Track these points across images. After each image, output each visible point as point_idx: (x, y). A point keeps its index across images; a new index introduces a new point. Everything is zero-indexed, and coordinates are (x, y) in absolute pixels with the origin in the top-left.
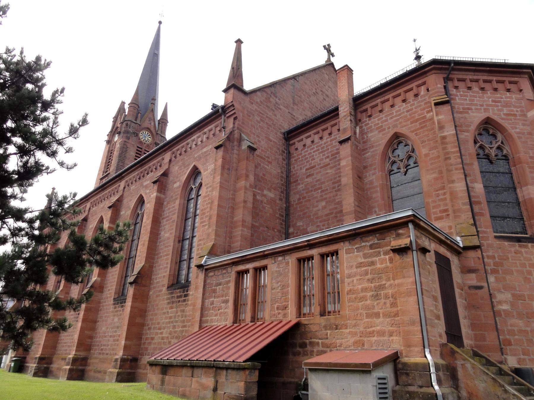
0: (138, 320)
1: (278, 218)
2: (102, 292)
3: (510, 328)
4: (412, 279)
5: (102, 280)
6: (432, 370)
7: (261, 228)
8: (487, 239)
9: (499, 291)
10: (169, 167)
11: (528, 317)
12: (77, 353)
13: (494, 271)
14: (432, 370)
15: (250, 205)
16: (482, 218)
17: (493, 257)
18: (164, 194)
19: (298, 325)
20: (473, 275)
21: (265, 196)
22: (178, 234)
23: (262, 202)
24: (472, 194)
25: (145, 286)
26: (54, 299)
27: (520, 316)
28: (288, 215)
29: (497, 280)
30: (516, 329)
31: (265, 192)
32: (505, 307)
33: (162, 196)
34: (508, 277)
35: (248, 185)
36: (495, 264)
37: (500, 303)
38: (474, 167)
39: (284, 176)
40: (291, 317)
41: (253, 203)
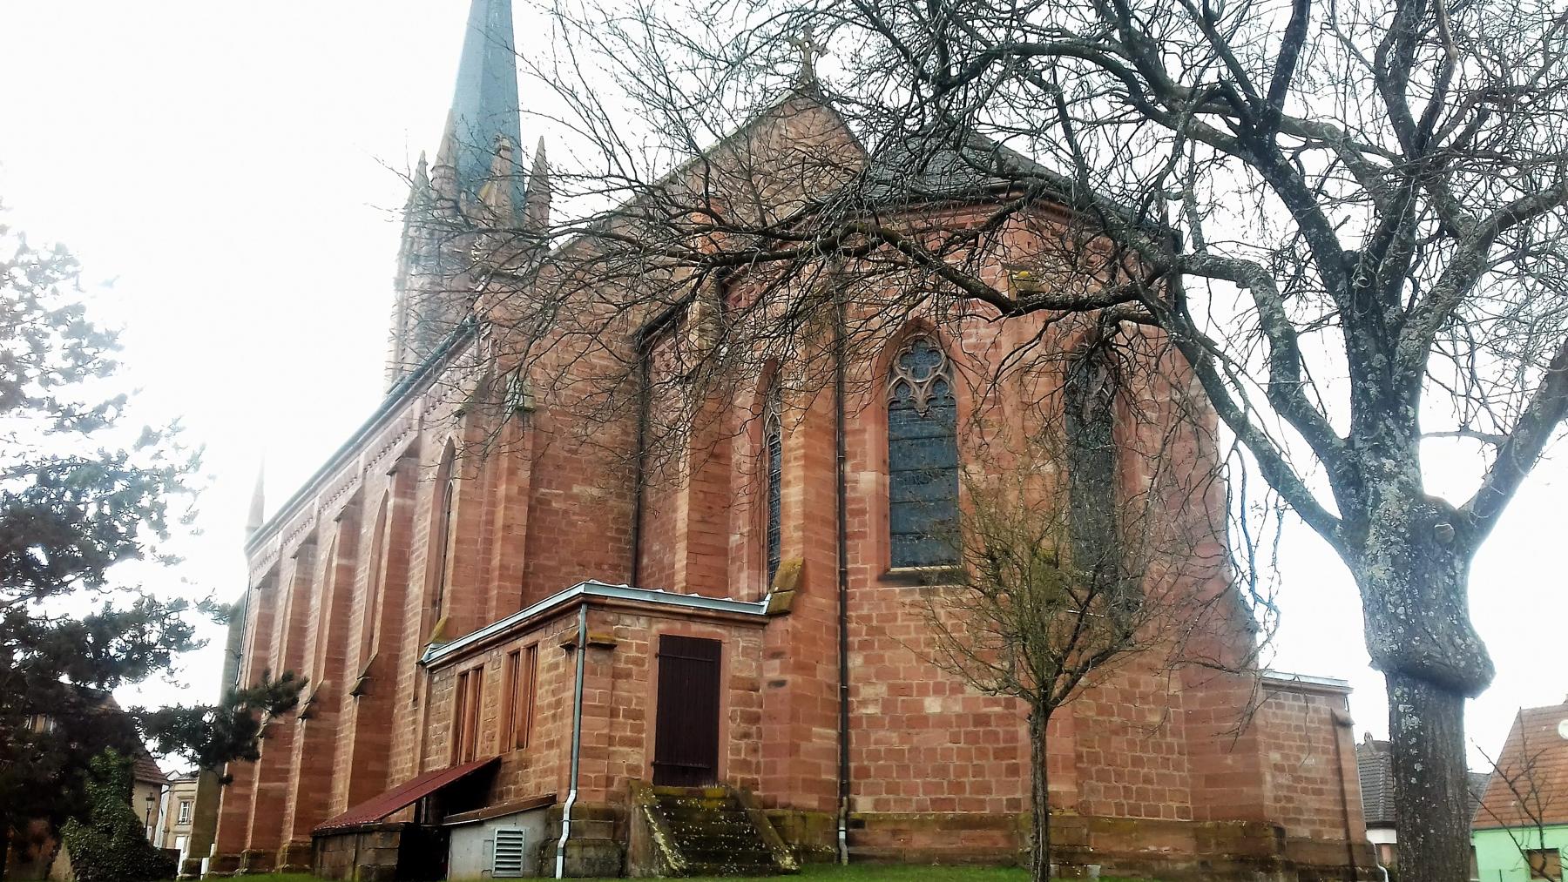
0: (373, 766)
1: (612, 539)
2: (338, 711)
3: (873, 747)
4: (571, 693)
5: (334, 684)
6: (566, 817)
7: (564, 570)
8: (863, 583)
9: (868, 682)
10: (419, 438)
11: (908, 726)
12: (299, 839)
13: (864, 645)
14: (566, 817)
15: (520, 532)
16: (860, 543)
17: (868, 618)
18: (413, 497)
19: (494, 766)
20: (777, 662)
21: (575, 498)
22: (431, 587)
23: (566, 512)
24: (849, 494)
25: (382, 698)
26: (1371, 540)
27: (895, 724)
28: (638, 530)
29: (868, 661)
30: (883, 748)
31: (576, 489)
32: (871, 710)
33: (409, 502)
34: (888, 654)
35: (515, 489)
36: (872, 631)
37: (864, 703)
38: (867, 436)
39: (632, 439)
40: (496, 755)
41: (529, 527)
